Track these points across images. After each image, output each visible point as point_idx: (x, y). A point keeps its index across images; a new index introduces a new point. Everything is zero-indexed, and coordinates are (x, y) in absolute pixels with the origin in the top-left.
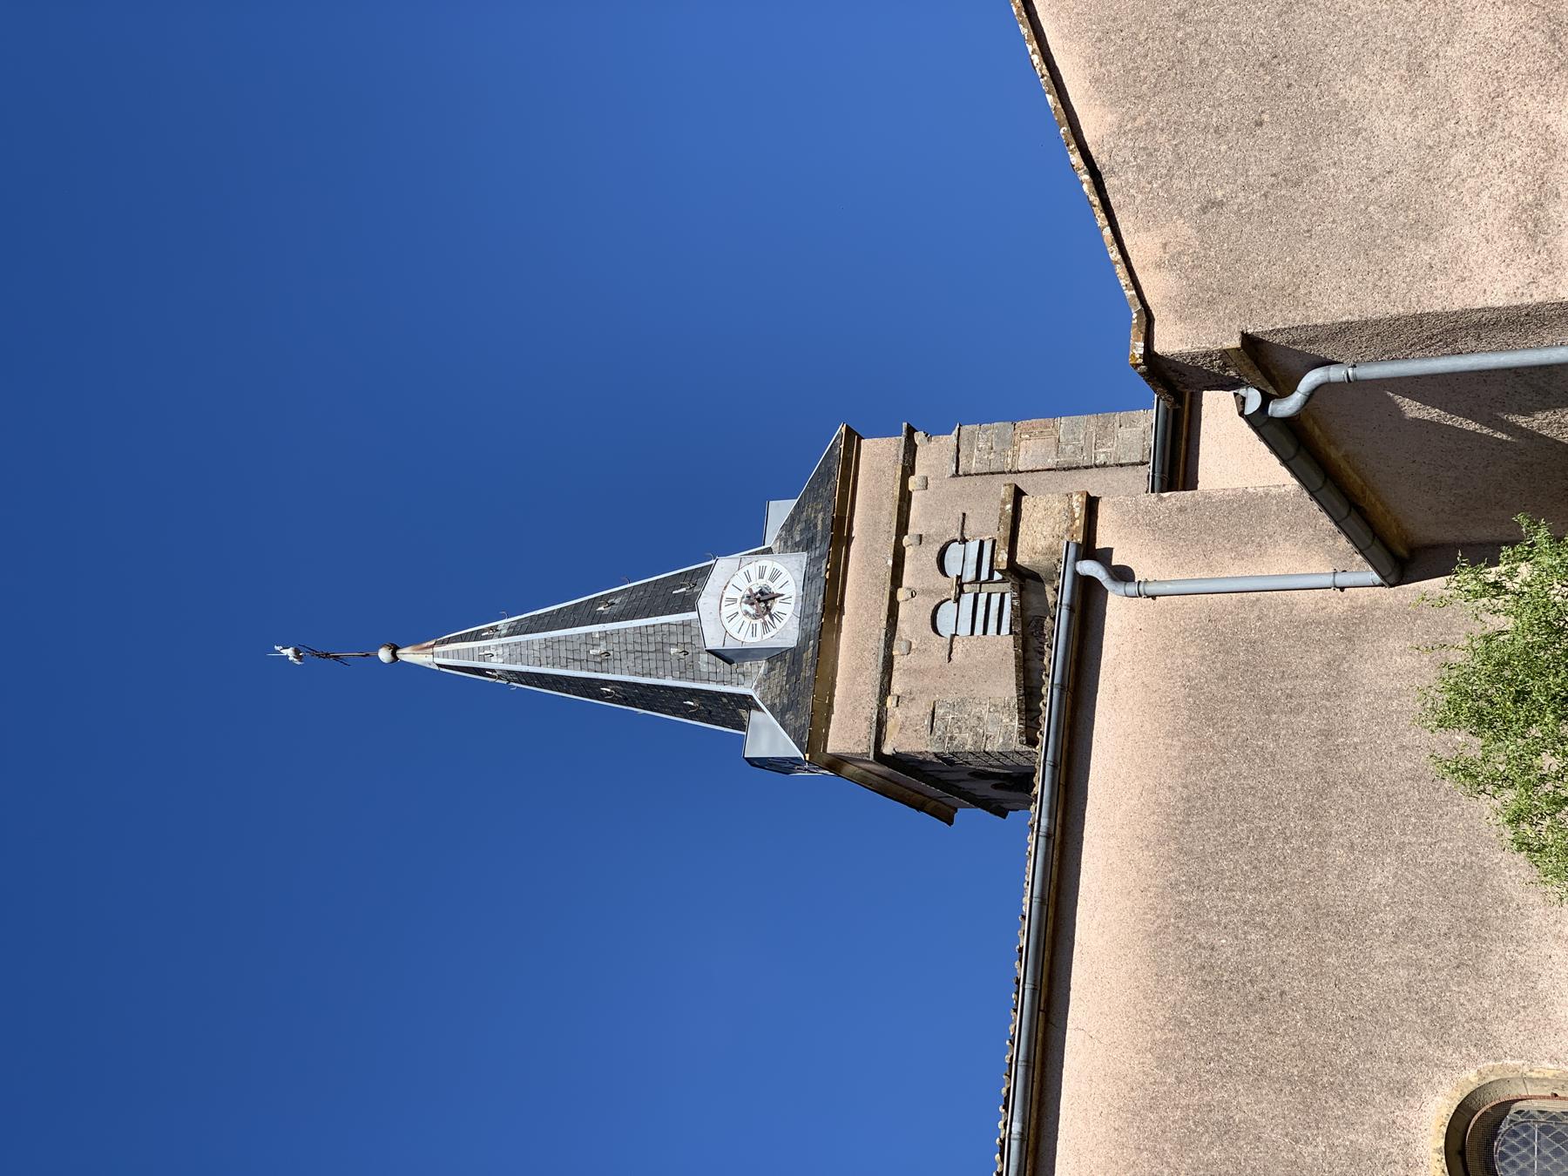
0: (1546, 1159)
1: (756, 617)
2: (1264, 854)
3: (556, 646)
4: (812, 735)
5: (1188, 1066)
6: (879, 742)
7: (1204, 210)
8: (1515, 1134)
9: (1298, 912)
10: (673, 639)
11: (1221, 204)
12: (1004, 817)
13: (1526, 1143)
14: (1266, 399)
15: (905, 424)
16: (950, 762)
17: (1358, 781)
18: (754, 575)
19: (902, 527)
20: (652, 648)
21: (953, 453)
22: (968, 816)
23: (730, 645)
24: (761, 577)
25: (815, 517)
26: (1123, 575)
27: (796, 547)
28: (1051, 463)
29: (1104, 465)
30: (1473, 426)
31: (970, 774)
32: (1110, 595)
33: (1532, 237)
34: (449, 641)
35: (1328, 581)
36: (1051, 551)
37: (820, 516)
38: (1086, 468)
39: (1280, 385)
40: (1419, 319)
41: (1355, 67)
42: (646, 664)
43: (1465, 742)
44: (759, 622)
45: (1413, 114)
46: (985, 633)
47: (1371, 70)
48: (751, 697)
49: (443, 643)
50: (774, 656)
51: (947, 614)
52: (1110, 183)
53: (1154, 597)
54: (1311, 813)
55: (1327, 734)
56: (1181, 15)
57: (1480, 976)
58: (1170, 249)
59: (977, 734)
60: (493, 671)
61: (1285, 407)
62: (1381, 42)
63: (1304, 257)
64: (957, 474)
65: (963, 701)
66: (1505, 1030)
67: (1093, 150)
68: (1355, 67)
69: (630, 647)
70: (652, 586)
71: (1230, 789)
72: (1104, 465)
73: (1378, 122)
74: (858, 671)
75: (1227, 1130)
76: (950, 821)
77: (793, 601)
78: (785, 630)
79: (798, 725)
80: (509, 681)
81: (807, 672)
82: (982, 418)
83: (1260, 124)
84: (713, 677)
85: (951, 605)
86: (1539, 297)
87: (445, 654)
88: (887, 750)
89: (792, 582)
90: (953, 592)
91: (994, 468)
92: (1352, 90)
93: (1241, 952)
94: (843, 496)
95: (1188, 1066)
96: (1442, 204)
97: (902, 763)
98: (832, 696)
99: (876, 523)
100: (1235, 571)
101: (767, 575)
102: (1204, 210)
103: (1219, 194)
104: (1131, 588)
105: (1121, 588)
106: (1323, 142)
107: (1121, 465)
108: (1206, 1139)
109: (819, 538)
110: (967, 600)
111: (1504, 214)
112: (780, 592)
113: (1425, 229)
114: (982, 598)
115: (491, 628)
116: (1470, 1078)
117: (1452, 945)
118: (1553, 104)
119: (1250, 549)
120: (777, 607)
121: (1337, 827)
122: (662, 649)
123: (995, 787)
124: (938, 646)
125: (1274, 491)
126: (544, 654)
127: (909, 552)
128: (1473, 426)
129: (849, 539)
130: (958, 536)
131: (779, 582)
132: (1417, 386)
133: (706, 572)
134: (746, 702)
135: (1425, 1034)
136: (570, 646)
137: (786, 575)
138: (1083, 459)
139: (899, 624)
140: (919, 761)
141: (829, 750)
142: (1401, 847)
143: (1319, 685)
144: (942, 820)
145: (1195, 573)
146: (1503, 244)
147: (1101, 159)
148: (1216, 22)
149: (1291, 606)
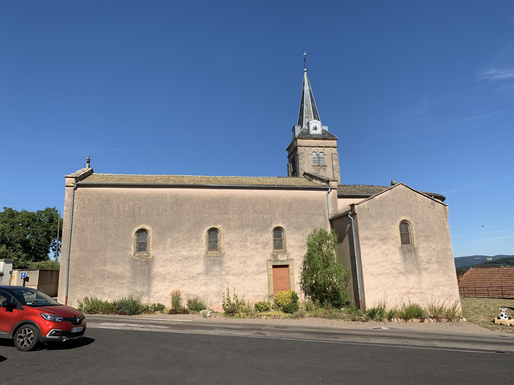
1: (313, 128)
4: (300, 137)
7: (368, 209)
10: (310, 115)
11: (369, 210)
12: (288, 157)
14: (350, 214)
15: (338, 138)
17: (310, 217)
18: (319, 127)
19: (325, 147)
22: (287, 154)
26: (329, 193)
27: (322, 132)
28: (334, 166)
29: (333, 172)
30: (347, 230)
32: (327, 192)
34: (308, 80)
35: (329, 214)
36: (331, 185)
40: (358, 229)
45: (376, 227)
47: (381, 223)
50: (308, 130)
51: (315, 154)
52: (371, 199)
54: (307, 213)
56: (387, 205)
65: (304, 157)
66: (289, 232)
68: (381, 222)
72: (333, 172)
73: (376, 224)
74: (307, 142)
75: (277, 206)
78: (312, 132)
85: (316, 154)
87: (306, 80)
88: (298, 147)
91: (333, 159)
92: (379, 222)
94: (329, 139)
96: (368, 230)
97: (296, 149)
99: (325, 143)
100: (330, 204)
102: (368, 209)
104: (327, 194)
105: (328, 193)
110: (317, 156)
111: (367, 236)
113: (366, 229)
114: (317, 158)
116: (285, 228)
117: (296, 226)
118: (377, 239)
120: (315, 130)
121: (306, 215)
122: (308, 113)
123: (292, 158)
124: (311, 153)
127: (322, 148)
128: (347, 230)
129: (324, 140)
131: (318, 131)
132: (351, 226)
133: (319, 120)
134: (302, 126)
138: (334, 170)
143: (319, 213)
145: (329, 200)
147: (373, 198)
149: (327, 210)
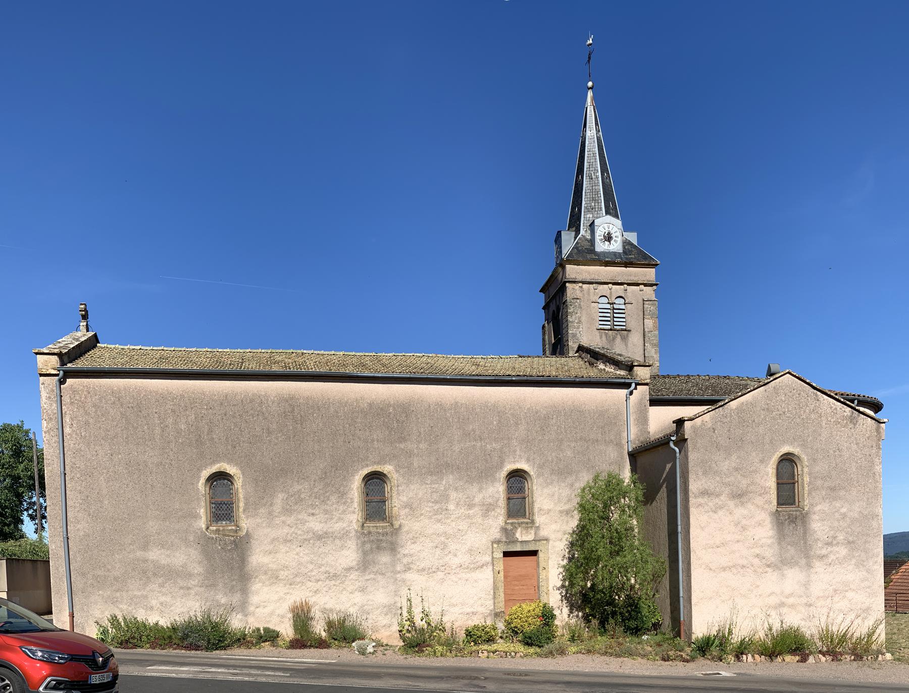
0: (516, 487)
1: (604, 235)
2: (572, 429)
3: (594, 158)
4: (571, 260)
5: (528, 415)
6: (569, 282)
8: (520, 481)
9: (561, 437)
10: (596, 204)
11: (714, 432)
13: (519, 483)
15: (659, 283)
16: (564, 303)
17: (588, 447)
19: (629, 284)
20: (594, 196)
21: (650, 299)
22: (541, 299)
23: (596, 228)
24: (616, 237)
25: (633, 254)
26: (631, 393)
27: (624, 247)
28: (646, 330)
29: (644, 345)
31: (558, 306)
33: (702, 493)
34: (595, 112)
35: (629, 440)
37: (633, 256)
38: (644, 340)
39: (676, 443)
40: (688, 472)
41: (739, 457)
42: (589, 194)
43: (604, 476)
44: (602, 237)
46: (600, 312)
48: (579, 233)
49: (594, 110)
50: (592, 241)
51: (604, 300)
52: (721, 408)
53: (626, 401)
55: (597, 441)
57: (551, 474)
58: (705, 423)
59: (573, 313)
60: (585, 131)
61: (672, 445)
62: (743, 462)
63: (702, 450)
64: (644, 301)
66: (541, 480)
67: (728, 404)
68: (739, 457)
69: (594, 187)
70: (611, 193)
71: (585, 421)
72: (644, 345)
73: (727, 463)
74: (589, 273)
75: (517, 424)
76: (540, 291)
77: (609, 248)
78: (601, 247)
79: (574, 254)
80: (582, 137)
81: (589, 256)
82: (660, 308)
83: (729, 439)
84: (585, 219)
85: (607, 301)
86: (690, 495)
88: (567, 285)
89: (614, 247)
90: (611, 302)
91: (645, 312)
92: (734, 457)
93: (552, 425)
94: (639, 264)
95: (528, 415)
96: (709, 476)
97: (562, 289)
98: (582, 265)
101: (616, 239)
103: (716, 432)
104: (628, 396)
105: (628, 393)
106: (724, 452)
107: (644, 351)
108: (514, 419)
109: (627, 257)
111: (706, 487)
112: (611, 244)
113: (705, 473)
114: (609, 311)
115: (599, 130)
116: (532, 473)
117: (556, 468)
118: (726, 495)
119: (636, 422)
120: (607, 243)
123: (554, 311)
124: (595, 298)
125: (649, 427)
126: (591, 153)
127: (622, 287)
130: (626, 302)
131: (614, 243)
134: (578, 231)
135: (539, 464)
136: (594, 163)
137: (616, 245)
138: (647, 339)
139: (602, 285)
140: (563, 293)
141: (567, 265)
142: (575, 457)
143: (607, 439)
144: (690, 557)
146: (701, 487)
147: (726, 406)
148: (752, 428)
149: (624, 431)
